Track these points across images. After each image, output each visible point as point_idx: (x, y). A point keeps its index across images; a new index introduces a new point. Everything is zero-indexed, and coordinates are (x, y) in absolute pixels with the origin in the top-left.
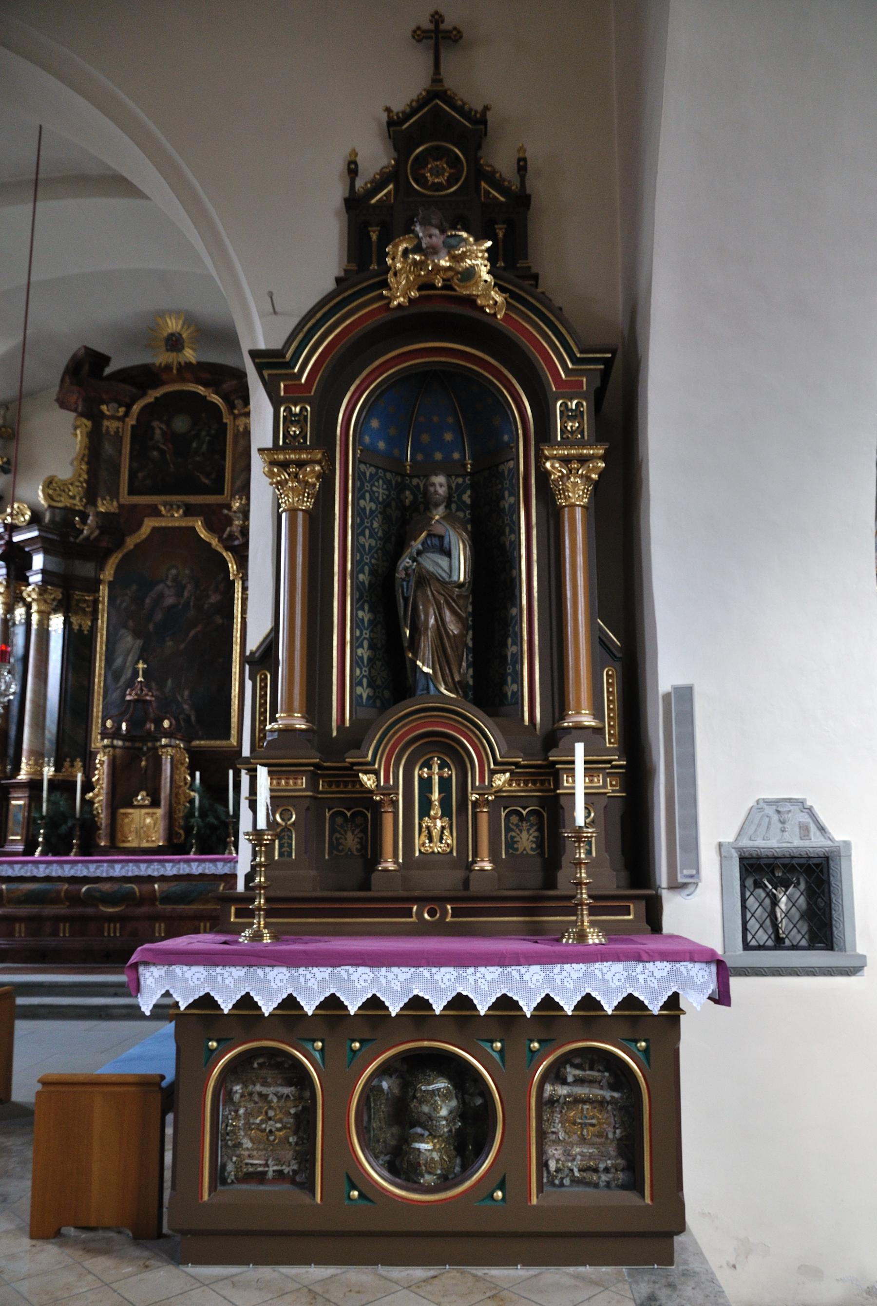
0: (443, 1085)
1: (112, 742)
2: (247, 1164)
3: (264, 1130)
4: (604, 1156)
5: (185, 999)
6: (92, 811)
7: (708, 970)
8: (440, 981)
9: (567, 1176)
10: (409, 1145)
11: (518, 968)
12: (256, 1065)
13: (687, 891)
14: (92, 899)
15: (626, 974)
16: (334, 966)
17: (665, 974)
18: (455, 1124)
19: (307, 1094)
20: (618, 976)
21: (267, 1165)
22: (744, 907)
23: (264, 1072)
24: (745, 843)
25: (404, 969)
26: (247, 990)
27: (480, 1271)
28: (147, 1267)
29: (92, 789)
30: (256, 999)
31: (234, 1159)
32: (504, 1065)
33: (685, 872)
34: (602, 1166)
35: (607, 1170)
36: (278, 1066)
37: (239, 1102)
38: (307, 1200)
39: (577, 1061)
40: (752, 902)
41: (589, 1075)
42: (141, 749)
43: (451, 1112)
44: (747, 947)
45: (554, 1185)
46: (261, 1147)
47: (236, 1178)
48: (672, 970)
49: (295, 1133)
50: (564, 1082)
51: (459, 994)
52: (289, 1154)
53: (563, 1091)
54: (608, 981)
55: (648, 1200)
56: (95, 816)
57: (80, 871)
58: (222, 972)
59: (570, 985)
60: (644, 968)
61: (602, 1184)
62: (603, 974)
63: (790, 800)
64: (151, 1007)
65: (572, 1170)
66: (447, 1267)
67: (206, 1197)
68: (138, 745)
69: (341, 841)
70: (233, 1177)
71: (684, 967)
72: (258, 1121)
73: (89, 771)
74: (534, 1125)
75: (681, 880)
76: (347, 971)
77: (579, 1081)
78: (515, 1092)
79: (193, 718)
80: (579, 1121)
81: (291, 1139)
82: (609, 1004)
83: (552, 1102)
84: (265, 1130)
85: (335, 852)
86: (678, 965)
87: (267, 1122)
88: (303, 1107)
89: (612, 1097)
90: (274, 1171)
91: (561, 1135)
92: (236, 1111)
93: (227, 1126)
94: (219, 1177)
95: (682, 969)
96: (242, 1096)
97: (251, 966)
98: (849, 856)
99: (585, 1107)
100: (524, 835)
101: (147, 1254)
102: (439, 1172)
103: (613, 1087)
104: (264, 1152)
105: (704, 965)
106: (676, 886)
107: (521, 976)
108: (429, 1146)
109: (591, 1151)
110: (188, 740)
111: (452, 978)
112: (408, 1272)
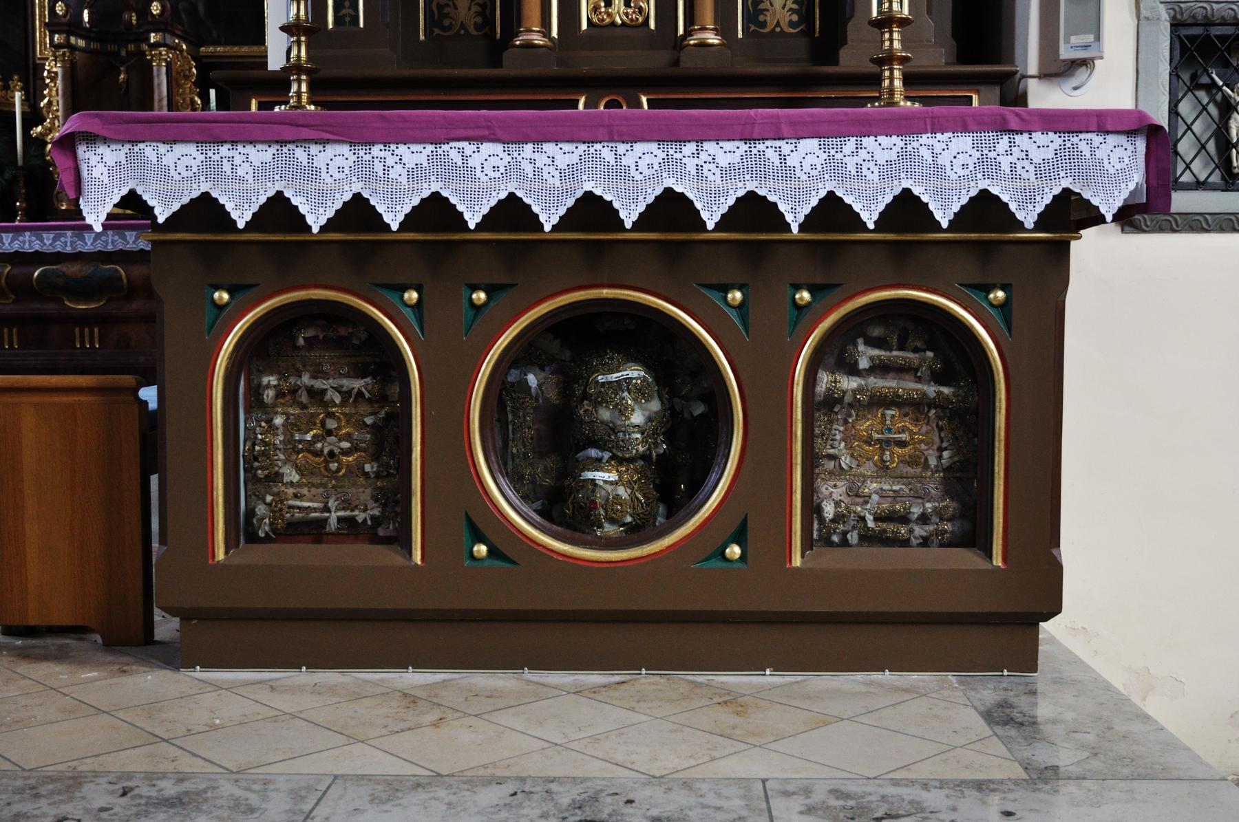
0: (636, 374)
1: (68, 39)
2: (291, 507)
3: (318, 454)
4: (921, 497)
5: (166, 204)
6: (43, 155)
7: (1130, 148)
8: (633, 168)
9: (854, 528)
10: (576, 478)
11: (777, 143)
12: (301, 342)
13: (1074, 82)
14: (53, 289)
15: (978, 155)
16: (437, 142)
17: (1051, 155)
18: (656, 444)
19: (395, 389)
20: (962, 159)
21: (327, 509)
23: (315, 354)
25: (567, 147)
26: (278, 187)
27: (702, 677)
28: (125, 672)
29: (41, 121)
30: (294, 202)
31: (269, 498)
32: (747, 332)
33: (1074, 40)
34: (916, 511)
35: (924, 519)
36: (340, 344)
37: (274, 405)
38: (399, 560)
39: (876, 332)
41: (897, 357)
42: (118, 53)
43: (650, 419)
45: (830, 544)
46: (317, 481)
47: (274, 530)
48: (1063, 147)
49: (375, 458)
50: (853, 370)
51: (668, 191)
52: (365, 495)
53: (849, 384)
54: (943, 167)
55: (998, 561)
56: (49, 164)
57: (28, 243)
58: (231, 153)
60: (1012, 144)
61: (914, 542)
62: (935, 156)
64: (103, 218)
65: (863, 519)
66: (644, 671)
67: (220, 555)
68: (111, 47)
69: (446, 10)
70: (267, 528)
72: (308, 437)
73: (32, 99)
74: (799, 433)
75: (1065, 53)
76: (461, 151)
77: (880, 368)
79: (201, 8)
80: (876, 436)
81: (368, 468)
82: (943, 208)
83: (832, 402)
84: (322, 451)
85: (437, 31)
86: (1075, 140)
87: (324, 439)
88: (387, 413)
89: (939, 393)
90: (340, 519)
91: (845, 461)
92: (269, 421)
93: (254, 445)
94: (243, 530)
95: (1083, 146)
96: (280, 394)
97: (283, 142)
99: (889, 412)
101: (125, 659)
102: (629, 519)
103: (938, 378)
104: (321, 490)
105: (1122, 139)
107: (783, 158)
108: (613, 477)
109: (896, 488)
110: (196, 42)
111: (655, 162)
112: (576, 677)
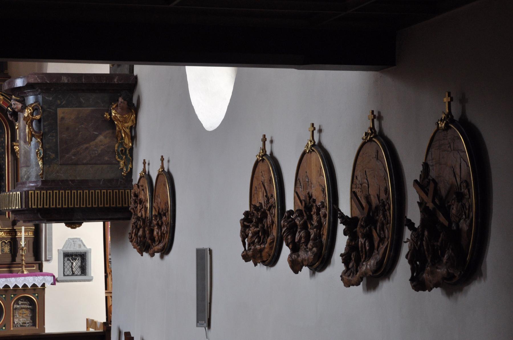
22: (64, 265)
24: (65, 249)
40: (66, 264)
44: (64, 275)
50: (19, 305)
53: (18, 306)
59: (21, 282)
63: (76, 238)
71: (46, 277)
75: (48, 259)
77: (22, 304)
78: (8, 306)
83: (16, 309)
98: (91, 252)
100: (6, 248)
103: (29, 305)
106: (46, 260)
